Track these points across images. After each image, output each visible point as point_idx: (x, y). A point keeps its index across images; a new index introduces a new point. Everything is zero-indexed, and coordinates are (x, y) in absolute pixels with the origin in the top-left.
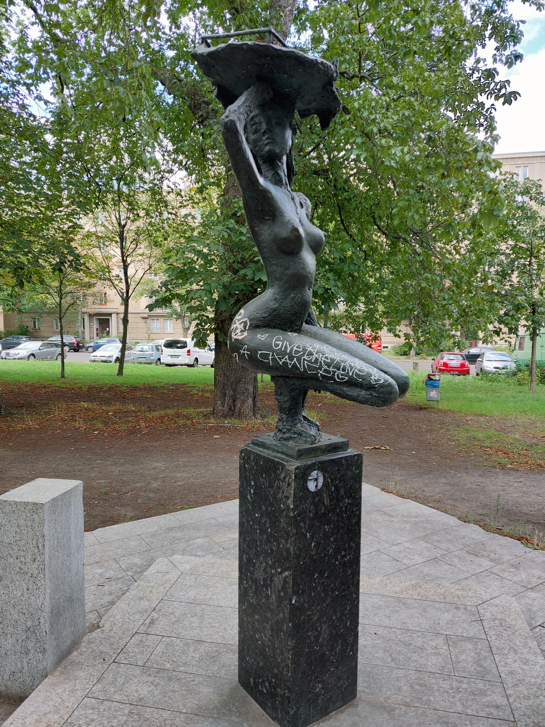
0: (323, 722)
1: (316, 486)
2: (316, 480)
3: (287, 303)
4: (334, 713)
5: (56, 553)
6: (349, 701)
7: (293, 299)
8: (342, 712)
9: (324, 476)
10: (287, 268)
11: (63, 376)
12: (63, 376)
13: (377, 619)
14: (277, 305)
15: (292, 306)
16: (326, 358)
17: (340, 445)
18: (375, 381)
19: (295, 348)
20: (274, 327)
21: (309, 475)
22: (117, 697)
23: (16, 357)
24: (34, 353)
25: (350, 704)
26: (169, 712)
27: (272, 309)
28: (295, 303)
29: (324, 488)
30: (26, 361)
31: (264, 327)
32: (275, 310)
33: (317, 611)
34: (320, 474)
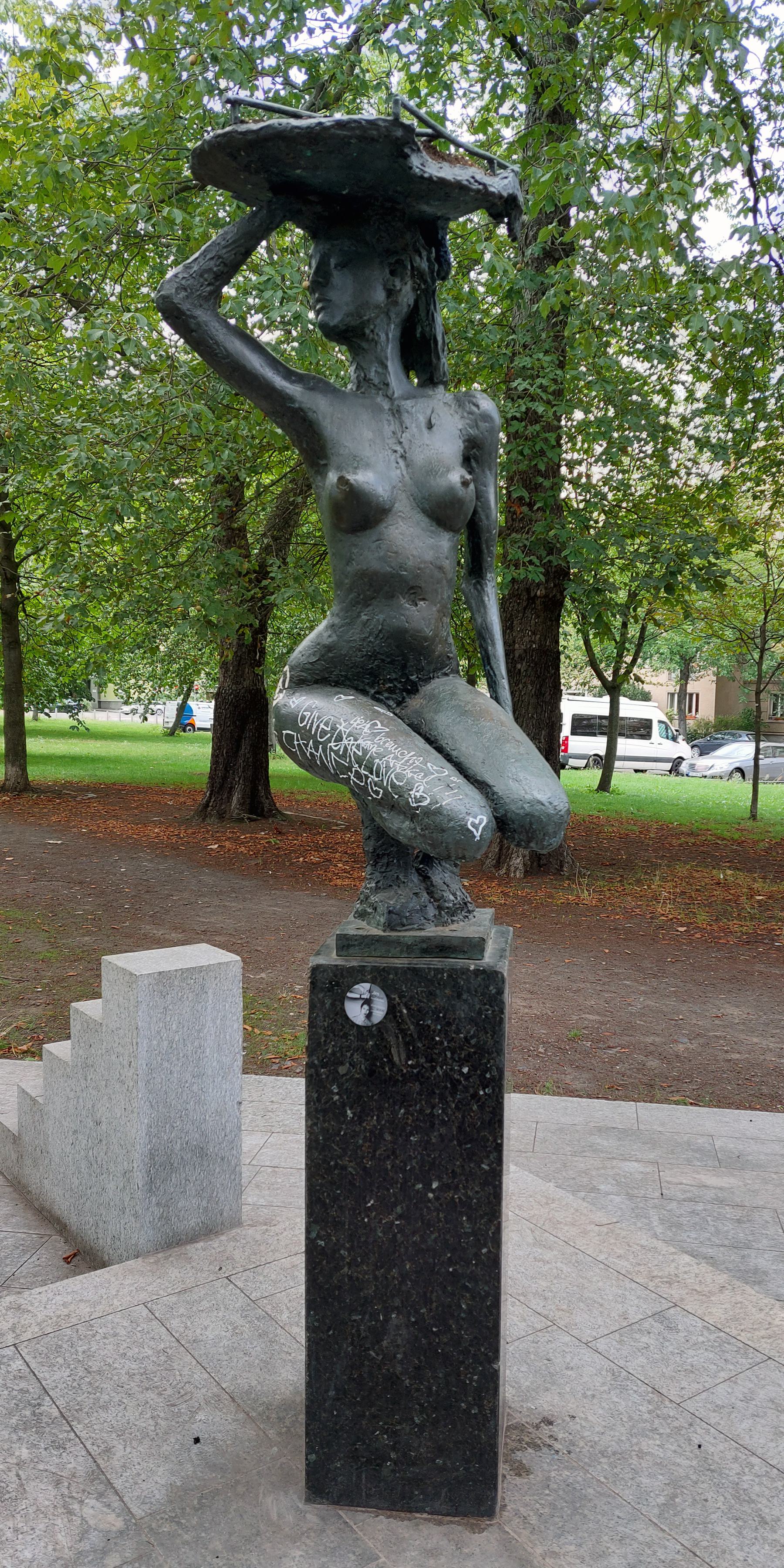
0: (389, 1517)
1: (369, 1016)
2: (368, 1002)
3: (355, 634)
4: (425, 1515)
5: (166, 1064)
6: (473, 1515)
7: (365, 624)
8: (440, 1523)
9: (390, 1000)
10: (349, 561)
11: (754, 816)
12: (754, 816)
13: (746, 1425)
14: (335, 638)
15: (364, 640)
16: (358, 746)
17: (455, 943)
18: (418, 801)
19: (322, 726)
20: (337, 684)
21: (349, 988)
22: (175, 1324)
23: (708, 773)
24: (743, 767)
25: (472, 1521)
26: (206, 1376)
27: (325, 646)
28: (370, 634)
29: (391, 1026)
30: (723, 783)
31: (316, 682)
32: (329, 648)
33: (376, 1278)
34: (378, 992)
